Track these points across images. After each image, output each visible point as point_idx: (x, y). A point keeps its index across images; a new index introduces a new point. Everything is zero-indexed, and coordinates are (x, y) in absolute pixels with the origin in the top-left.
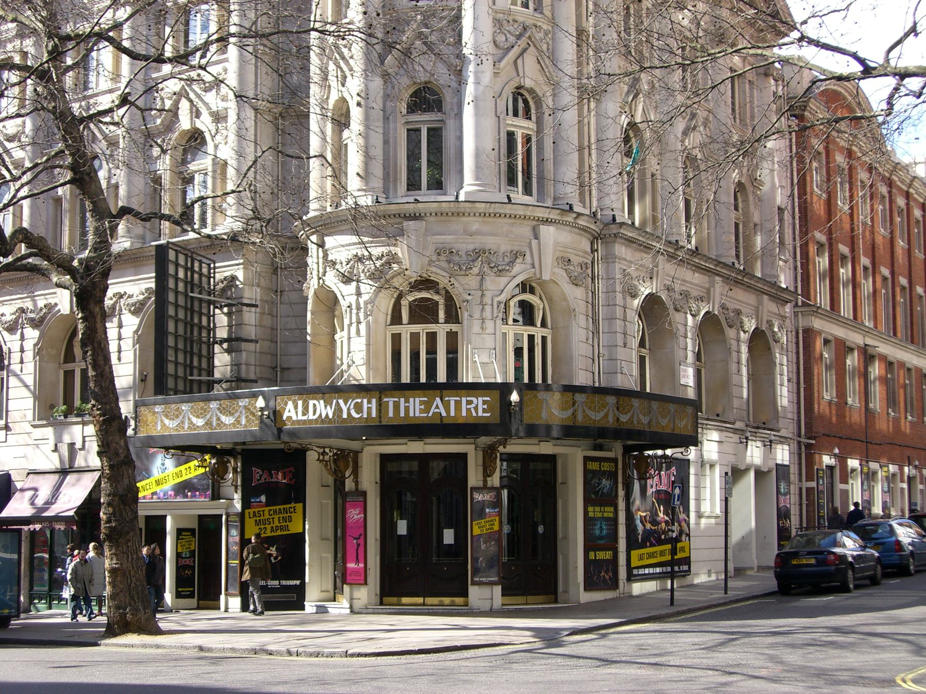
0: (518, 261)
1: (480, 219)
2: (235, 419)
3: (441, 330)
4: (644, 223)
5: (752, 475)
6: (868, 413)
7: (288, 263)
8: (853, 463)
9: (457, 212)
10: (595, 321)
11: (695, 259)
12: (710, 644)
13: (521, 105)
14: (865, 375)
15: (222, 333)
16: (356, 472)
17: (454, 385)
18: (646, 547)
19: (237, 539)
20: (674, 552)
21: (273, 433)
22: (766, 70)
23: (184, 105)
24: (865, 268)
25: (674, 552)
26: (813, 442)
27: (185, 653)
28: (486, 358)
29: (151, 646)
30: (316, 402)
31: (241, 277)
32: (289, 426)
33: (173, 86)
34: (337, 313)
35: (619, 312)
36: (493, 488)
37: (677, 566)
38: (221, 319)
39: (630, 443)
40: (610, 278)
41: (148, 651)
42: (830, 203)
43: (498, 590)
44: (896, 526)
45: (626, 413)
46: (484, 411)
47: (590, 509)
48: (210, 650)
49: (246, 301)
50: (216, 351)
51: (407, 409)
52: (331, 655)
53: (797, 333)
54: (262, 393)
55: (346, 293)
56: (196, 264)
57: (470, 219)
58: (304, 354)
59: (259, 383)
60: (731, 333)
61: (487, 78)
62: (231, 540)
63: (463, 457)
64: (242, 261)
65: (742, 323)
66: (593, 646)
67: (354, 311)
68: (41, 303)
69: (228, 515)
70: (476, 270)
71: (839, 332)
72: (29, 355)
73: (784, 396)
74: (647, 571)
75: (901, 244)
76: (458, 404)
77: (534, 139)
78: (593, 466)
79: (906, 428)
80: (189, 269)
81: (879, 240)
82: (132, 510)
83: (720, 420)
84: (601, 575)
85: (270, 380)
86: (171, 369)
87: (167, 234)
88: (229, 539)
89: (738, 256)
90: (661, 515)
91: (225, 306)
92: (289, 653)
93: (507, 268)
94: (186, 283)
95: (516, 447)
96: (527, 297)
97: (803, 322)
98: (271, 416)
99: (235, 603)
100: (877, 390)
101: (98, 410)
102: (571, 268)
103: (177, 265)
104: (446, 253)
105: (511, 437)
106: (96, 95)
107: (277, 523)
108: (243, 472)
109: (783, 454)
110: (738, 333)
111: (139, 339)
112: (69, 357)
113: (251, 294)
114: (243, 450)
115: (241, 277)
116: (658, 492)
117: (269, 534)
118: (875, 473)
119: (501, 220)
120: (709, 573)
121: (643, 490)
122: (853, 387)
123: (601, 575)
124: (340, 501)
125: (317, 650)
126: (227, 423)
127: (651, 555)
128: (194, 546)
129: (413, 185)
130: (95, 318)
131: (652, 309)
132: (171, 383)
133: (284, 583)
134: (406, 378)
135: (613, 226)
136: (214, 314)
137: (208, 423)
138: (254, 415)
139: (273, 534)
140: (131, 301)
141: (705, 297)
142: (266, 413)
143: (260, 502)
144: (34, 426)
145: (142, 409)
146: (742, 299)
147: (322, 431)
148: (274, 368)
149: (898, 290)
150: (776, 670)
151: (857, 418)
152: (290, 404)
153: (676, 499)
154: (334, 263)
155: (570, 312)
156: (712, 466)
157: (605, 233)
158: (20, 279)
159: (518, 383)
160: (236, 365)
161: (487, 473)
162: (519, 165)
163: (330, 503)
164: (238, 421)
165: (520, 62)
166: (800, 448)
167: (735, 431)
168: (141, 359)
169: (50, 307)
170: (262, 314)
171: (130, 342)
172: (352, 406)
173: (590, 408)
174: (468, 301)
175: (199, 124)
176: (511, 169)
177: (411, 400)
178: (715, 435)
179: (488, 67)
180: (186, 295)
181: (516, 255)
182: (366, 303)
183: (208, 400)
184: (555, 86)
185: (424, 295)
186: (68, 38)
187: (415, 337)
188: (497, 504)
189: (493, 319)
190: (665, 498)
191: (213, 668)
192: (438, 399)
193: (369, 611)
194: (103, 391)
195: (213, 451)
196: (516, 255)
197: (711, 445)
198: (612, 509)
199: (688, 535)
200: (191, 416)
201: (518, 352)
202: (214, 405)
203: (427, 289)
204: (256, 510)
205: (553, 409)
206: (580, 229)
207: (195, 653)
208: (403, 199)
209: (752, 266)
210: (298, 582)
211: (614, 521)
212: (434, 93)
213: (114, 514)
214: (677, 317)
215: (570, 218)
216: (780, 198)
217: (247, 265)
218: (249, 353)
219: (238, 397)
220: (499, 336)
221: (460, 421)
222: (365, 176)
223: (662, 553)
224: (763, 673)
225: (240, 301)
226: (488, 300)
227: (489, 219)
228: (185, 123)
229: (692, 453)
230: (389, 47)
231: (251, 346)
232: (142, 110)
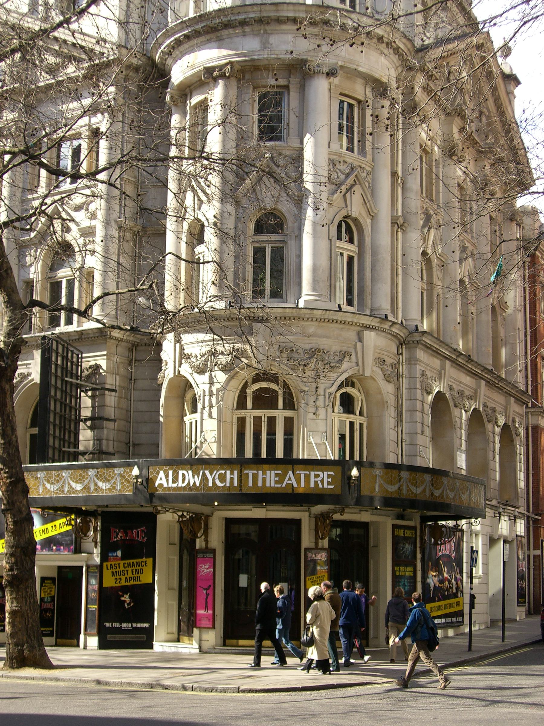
0: (345, 359)
1: (316, 324)
2: (112, 484)
9: (300, 316)
15: (86, 413)
16: (206, 533)
17: (290, 461)
18: (435, 601)
19: (96, 587)
21: (145, 497)
26: (540, 518)
28: (317, 439)
29: (51, 679)
30: (185, 472)
31: (104, 367)
32: (160, 492)
35: (419, 404)
38: (86, 401)
40: (412, 378)
41: (49, 683)
45: (439, 489)
46: (329, 483)
48: (107, 683)
49: (108, 386)
50: (81, 428)
51: (264, 480)
52: (225, 691)
55: (200, 384)
57: (308, 323)
58: (157, 433)
59: (116, 456)
60: (489, 426)
62: (90, 588)
63: (297, 523)
64: (105, 353)
65: (497, 419)
67: (207, 398)
69: (88, 567)
70: (312, 366)
76: (307, 477)
78: (400, 533)
80: (65, 358)
82: (31, 560)
85: (125, 453)
88: (88, 587)
91: (90, 390)
92: (184, 688)
93: (338, 365)
94: (62, 369)
95: (350, 515)
96: (349, 390)
97: (532, 421)
98: (144, 482)
99: (93, 641)
101: (5, 473)
102: (385, 367)
104: (288, 352)
105: (347, 506)
108: (102, 530)
109: (521, 527)
110: (494, 427)
113: (112, 381)
114: (103, 512)
115: (104, 367)
117: (123, 583)
119: (332, 325)
124: (186, 557)
125: (211, 686)
126: (104, 488)
128: (54, 592)
129: (258, 293)
130: (5, 394)
133: (135, 625)
134: (249, 453)
135: (416, 334)
136: (80, 397)
137: (86, 488)
138: (128, 481)
139: (127, 584)
141: (473, 397)
142: (140, 480)
143: (117, 556)
154: (188, 357)
155: (383, 404)
156: (476, 535)
157: (409, 340)
160: (98, 440)
162: (355, 280)
164: (114, 487)
165: (348, 196)
166: (528, 522)
170: (120, 397)
172: (217, 477)
173: (412, 484)
174: (305, 391)
175: (69, 237)
177: (268, 473)
180: (63, 380)
181: (344, 355)
182: (218, 391)
184: (373, 217)
185: (264, 385)
187: (257, 420)
192: (290, 473)
193: (217, 651)
195: (78, 512)
196: (344, 355)
198: (412, 569)
200: (71, 482)
201: (342, 437)
203: (269, 380)
204: (113, 563)
205: (377, 486)
206: (392, 335)
210: (147, 625)
212: (276, 217)
213: (16, 563)
214: (456, 412)
215: (386, 326)
217: (109, 357)
218: (109, 430)
219: (113, 466)
225: (103, 386)
226: (321, 391)
227: (324, 324)
231: (111, 425)
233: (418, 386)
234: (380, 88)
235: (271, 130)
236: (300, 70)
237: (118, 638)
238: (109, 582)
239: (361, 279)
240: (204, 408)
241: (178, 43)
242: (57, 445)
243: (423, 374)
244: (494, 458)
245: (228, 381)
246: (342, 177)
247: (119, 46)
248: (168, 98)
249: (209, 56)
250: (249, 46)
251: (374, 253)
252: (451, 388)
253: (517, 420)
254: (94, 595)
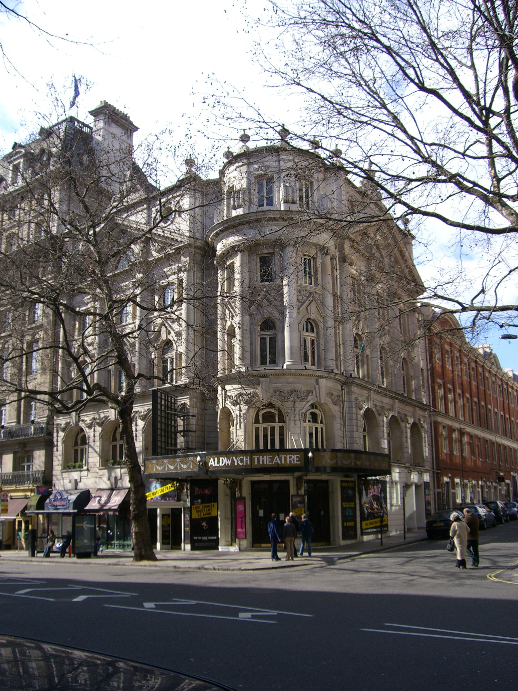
2: (187, 466)
3: (277, 425)
4: (364, 376)
5: (414, 487)
6: (463, 458)
7: (208, 399)
8: (457, 480)
9: (283, 373)
10: (344, 421)
11: (382, 392)
12: (402, 562)
13: (309, 326)
14: (461, 441)
15: (181, 428)
16: (240, 489)
17: (283, 450)
19: (189, 519)
20: (382, 521)
22: (415, 309)
23: (163, 329)
24: (459, 394)
25: (382, 521)
27: (169, 569)
31: (189, 404)
32: (211, 469)
33: (159, 321)
34: (231, 418)
35: (354, 416)
36: (301, 495)
37: (383, 528)
38: (180, 422)
39: (361, 474)
40: (350, 402)
41: (152, 568)
42: (443, 367)
44: (478, 508)
46: (297, 461)
47: (344, 503)
48: (179, 568)
51: (263, 461)
53: (431, 424)
54: (199, 454)
55: (235, 410)
56: (169, 398)
58: (217, 437)
60: (403, 424)
61: (295, 315)
63: (287, 482)
65: (407, 420)
66: (349, 564)
68: (102, 416)
70: (291, 399)
71: (449, 423)
72: (97, 438)
73: (426, 451)
74: (369, 531)
75: (474, 383)
76: (286, 458)
77: (315, 341)
79: (479, 464)
80: (166, 400)
81: (465, 383)
83: (399, 463)
84: (349, 533)
86: (159, 444)
87: (156, 385)
88: (184, 519)
89: (404, 391)
90: (375, 505)
92: (214, 569)
94: (165, 406)
95: (311, 477)
96: (314, 410)
99: (188, 547)
100: (466, 448)
103: (161, 399)
104: (278, 392)
106: (125, 326)
107: (206, 512)
109: (427, 478)
111: (144, 430)
112: (114, 439)
113: (193, 411)
115: (189, 404)
116: (373, 495)
117: (202, 516)
118: (467, 485)
120: (396, 531)
121: (367, 494)
122: (456, 446)
123: (349, 533)
124: (233, 502)
127: (371, 524)
128: (170, 521)
129: (263, 362)
131: (369, 415)
132: (159, 450)
133: (209, 538)
134: (262, 447)
137: (176, 468)
140: (141, 414)
144: (100, 469)
145: (147, 462)
146: (408, 409)
147: (225, 471)
148: (203, 443)
149: (474, 404)
150: (433, 573)
151: (458, 460)
152: (212, 459)
153: (381, 499)
155: (333, 417)
156: (396, 483)
157: (347, 381)
158: (94, 405)
159: (311, 449)
160: (186, 442)
161: (298, 489)
162: (309, 354)
163: (229, 502)
164: (189, 467)
165: (309, 308)
166: (434, 475)
167: (406, 467)
168: (145, 440)
169: (106, 417)
170: (198, 420)
171: (141, 432)
176: (306, 354)
178: (397, 470)
179: (295, 311)
181: (309, 392)
182: (243, 414)
183: (175, 457)
186: (116, 302)
187: (265, 429)
188: (302, 502)
189: (300, 420)
190: (376, 498)
191: (182, 576)
194: (132, 454)
195: (178, 480)
196: (309, 392)
197: (396, 474)
199: (387, 514)
201: (311, 435)
202: (178, 460)
205: (327, 460)
207: (172, 569)
208: (259, 368)
209: (411, 395)
210: (215, 538)
211: (354, 509)
212: (272, 322)
213: (136, 508)
214: (380, 418)
215: (332, 375)
216: (422, 364)
218: (192, 436)
219: (189, 456)
220: (302, 428)
221: (287, 466)
222: (242, 359)
223: (376, 522)
224: (427, 575)
226: (297, 412)
228: (164, 337)
229: (388, 478)
230: (252, 302)
231: (193, 434)
232: (147, 332)
233: (354, 406)
234: (324, 250)
235: (267, 276)
236: (280, 245)
237: (201, 544)
238: (195, 516)
240: (237, 424)
241: (217, 234)
242: (163, 446)
243: (356, 399)
244: (407, 441)
245: (248, 410)
246: (305, 298)
247: (190, 237)
248: (215, 262)
249: (232, 240)
250: (252, 234)
252: (376, 405)
253: (422, 419)
254: (188, 523)
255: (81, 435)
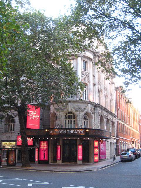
3: (73, 120)
43: (82, 161)
51: (71, 132)
76: (79, 132)
239: (87, 94)
251: (90, 90)
255: (55, 116)
